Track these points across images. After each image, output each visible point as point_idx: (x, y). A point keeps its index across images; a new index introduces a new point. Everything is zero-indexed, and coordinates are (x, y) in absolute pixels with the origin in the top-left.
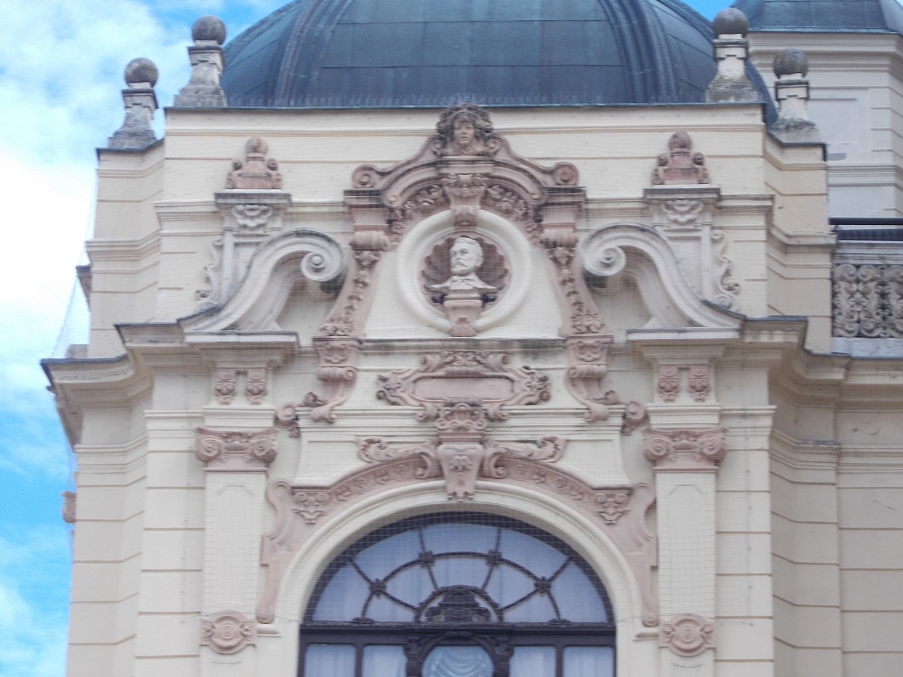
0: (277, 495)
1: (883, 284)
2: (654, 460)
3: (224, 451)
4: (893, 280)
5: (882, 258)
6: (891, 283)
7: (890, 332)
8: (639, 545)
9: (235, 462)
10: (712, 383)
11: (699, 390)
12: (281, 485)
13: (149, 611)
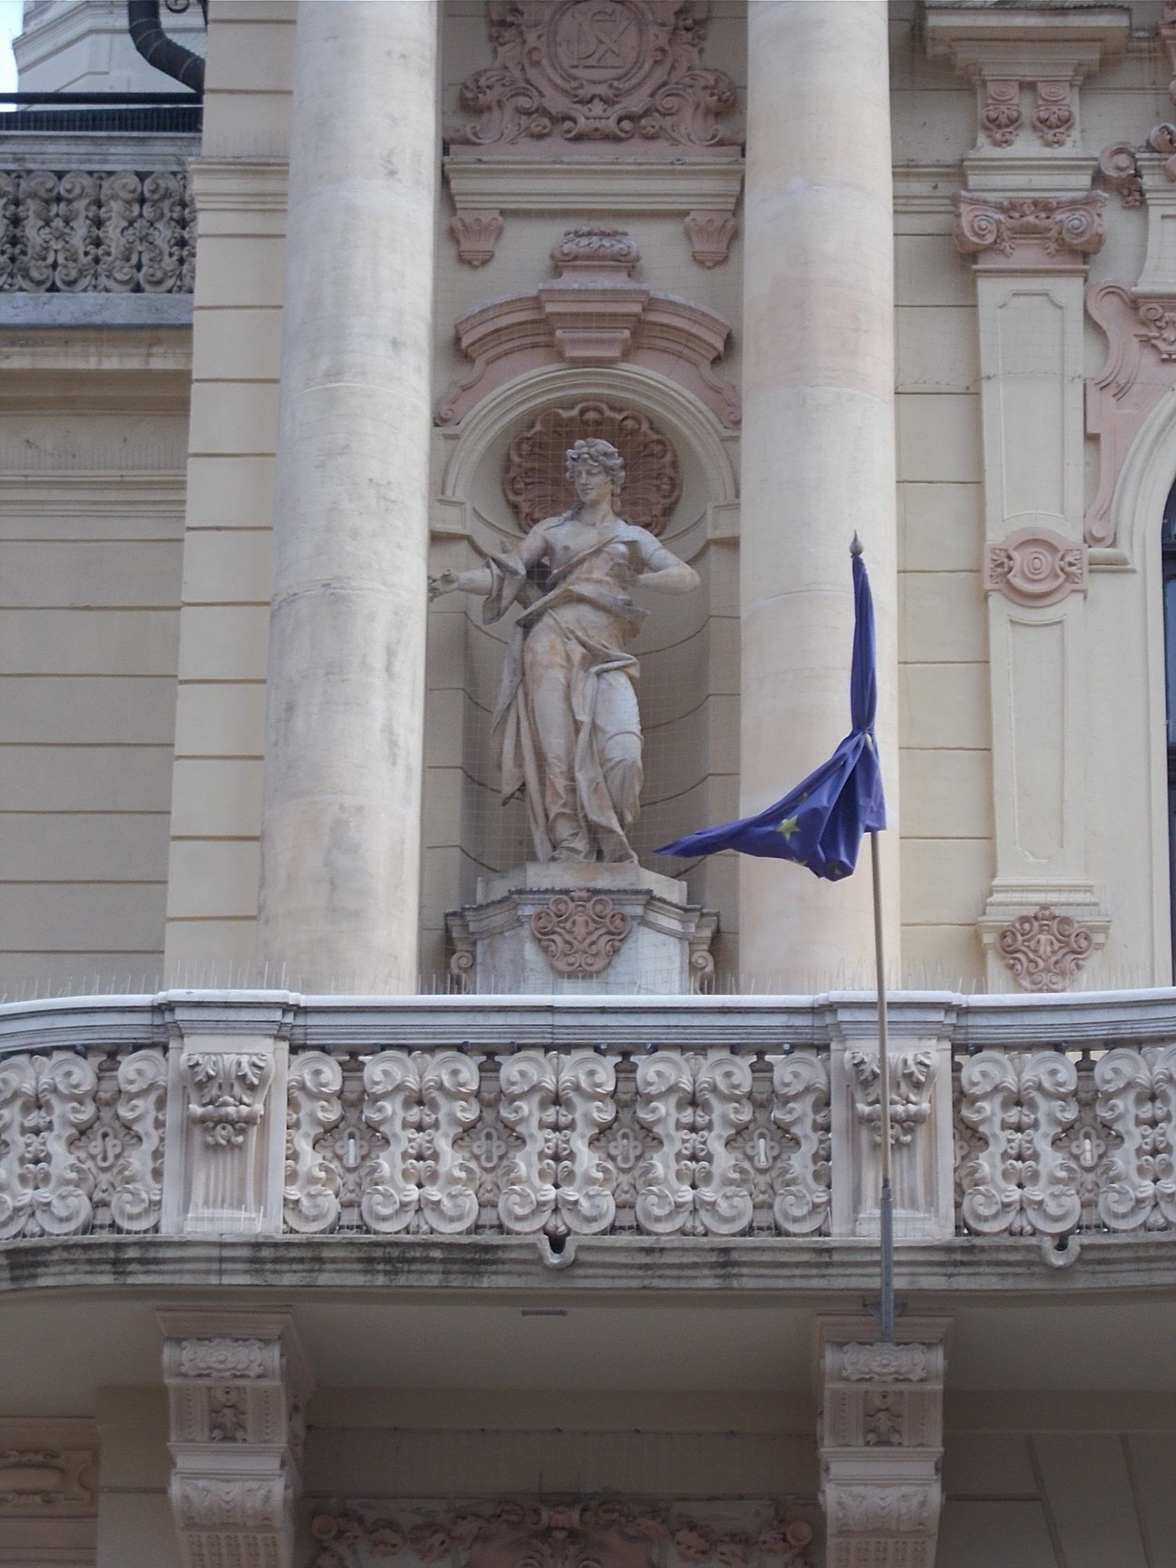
0: (1108, 312)
1: (17, 202)
3: (1007, 234)
4: (33, 195)
5: (18, 159)
6: (29, 201)
7: (19, 281)
12: (1112, 291)
13: (13, 605)
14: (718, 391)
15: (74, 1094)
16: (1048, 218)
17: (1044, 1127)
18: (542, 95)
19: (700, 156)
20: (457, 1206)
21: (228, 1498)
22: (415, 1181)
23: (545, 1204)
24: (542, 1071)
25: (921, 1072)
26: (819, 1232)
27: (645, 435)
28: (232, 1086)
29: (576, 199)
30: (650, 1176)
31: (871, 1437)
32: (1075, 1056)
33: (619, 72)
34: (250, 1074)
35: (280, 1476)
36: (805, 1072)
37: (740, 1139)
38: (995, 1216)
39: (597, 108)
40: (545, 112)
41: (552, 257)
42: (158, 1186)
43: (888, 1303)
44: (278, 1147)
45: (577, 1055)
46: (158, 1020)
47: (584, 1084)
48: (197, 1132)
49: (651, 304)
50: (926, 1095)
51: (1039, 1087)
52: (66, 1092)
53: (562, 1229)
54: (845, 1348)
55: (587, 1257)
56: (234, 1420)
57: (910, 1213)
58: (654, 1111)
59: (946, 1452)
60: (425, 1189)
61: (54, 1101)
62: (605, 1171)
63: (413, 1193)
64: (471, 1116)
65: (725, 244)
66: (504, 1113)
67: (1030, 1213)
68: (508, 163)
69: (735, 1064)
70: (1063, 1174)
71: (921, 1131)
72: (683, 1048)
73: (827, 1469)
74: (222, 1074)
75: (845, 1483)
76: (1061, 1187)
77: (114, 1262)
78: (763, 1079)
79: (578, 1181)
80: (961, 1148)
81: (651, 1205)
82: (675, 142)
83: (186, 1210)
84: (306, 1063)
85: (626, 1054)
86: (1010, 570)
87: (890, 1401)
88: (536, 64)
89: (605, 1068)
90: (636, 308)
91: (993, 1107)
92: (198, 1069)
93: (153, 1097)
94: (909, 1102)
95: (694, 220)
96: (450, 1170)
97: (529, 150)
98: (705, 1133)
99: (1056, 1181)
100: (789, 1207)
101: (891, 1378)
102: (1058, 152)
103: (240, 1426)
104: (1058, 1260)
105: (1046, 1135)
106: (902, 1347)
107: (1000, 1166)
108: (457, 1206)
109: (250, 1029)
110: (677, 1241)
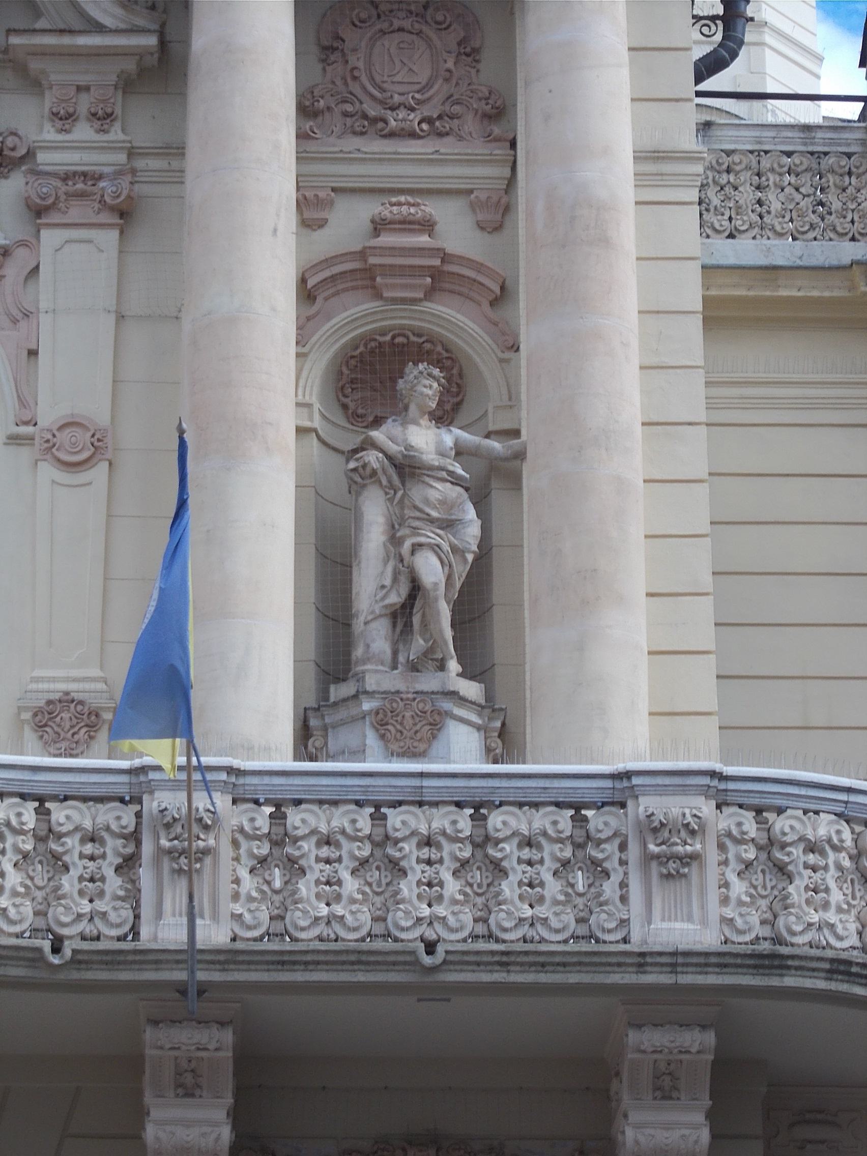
2: (38, 211)
8: (15, 321)
9: (76, 212)
10: (118, 111)
11: (103, 119)
14: (496, 324)
15: (561, 838)
16: (94, 185)
17: (548, 862)
18: (361, 103)
19: (480, 148)
20: (255, 918)
21: (189, 1139)
22: (325, 901)
23: (524, 919)
24: (519, 820)
25: (209, 818)
26: (625, 940)
27: (439, 354)
28: (679, 831)
29: (340, 179)
30: (296, 896)
31: (180, 1091)
32: (268, 810)
33: (417, 87)
34: (692, 822)
35: (706, 1125)
36: (513, 822)
37: (747, 872)
38: (802, 932)
39: (402, 114)
40: (365, 116)
41: (373, 221)
42: (626, 908)
43: (192, 992)
44: (225, 875)
45: (343, 808)
46: (134, 780)
47: (247, 828)
48: (654, 864)
49: (446, 257)
50: (698, 839)
51: (545, 834)
52: (117, 830)
53: (434, 937)
54: (643, 1029)
55: (450, 958)
56: (193, 1081)
57: (203, 922)
58: (299, 848)
59: (235, 1101)
60: (334, 907)
61: (543, 841)
62: (364, 893)
63: (324, 911)
64: (366, 853)
65: (500, 216)
66: (491, 851)
67: (539, 927)
68: (326, 153)
69: (743, 816)
70: (562, 898)
71: (208, 860)
72: (321, 802)
73: (626, 1116)
74: (671, 822)
75: (638, 1126)
76: (459, 906)
77: (640, 965)
78: (763, 829)
79: (344, 900)
80: (48, 871)
81: (499, 918)
82: (461, 138)
83: (649, 923)
84: (545, 815)
85: (278, 805)
86: (54, 445)
87: (193, 1064)
88: (355, 78)
89: (28, 811)
90: (437, 262)
91: (309, 846)
92: (653, 818)
93: (617, 842)
94: (686, 843)
95: (477, 197)
96: (351, 892)
97: (353, 143)
98: (336, 865)
99: (556, 903)
100: (600, 919)
101: (194, 1047)
102: (105, 137)
103: (199, 1086)
104: (427, 960)
105: (549, 869)
106: (684, 1028)
107: (314, 890)
108: (255, 918)
109: (684, 790)
110: (520, 947)
